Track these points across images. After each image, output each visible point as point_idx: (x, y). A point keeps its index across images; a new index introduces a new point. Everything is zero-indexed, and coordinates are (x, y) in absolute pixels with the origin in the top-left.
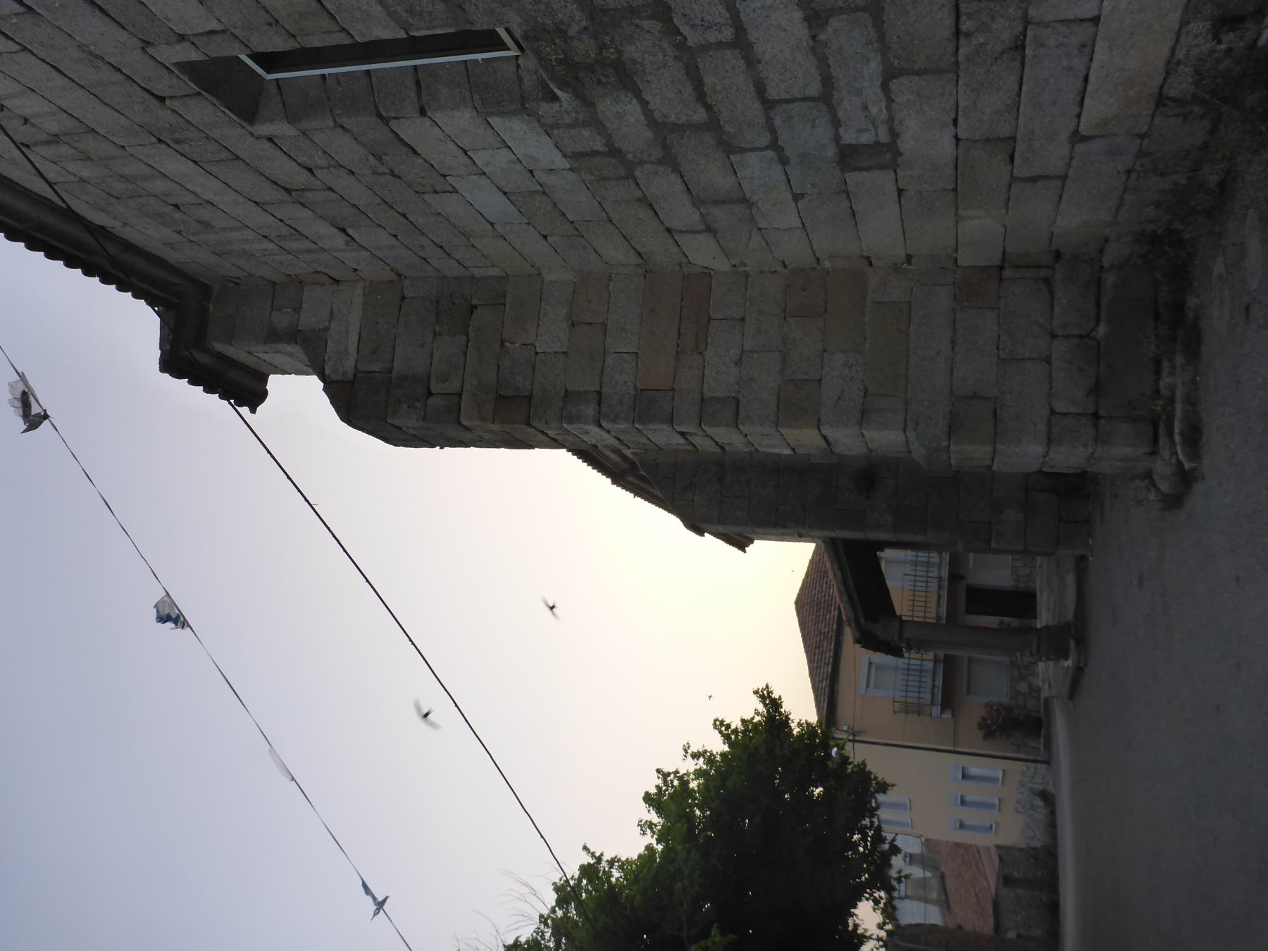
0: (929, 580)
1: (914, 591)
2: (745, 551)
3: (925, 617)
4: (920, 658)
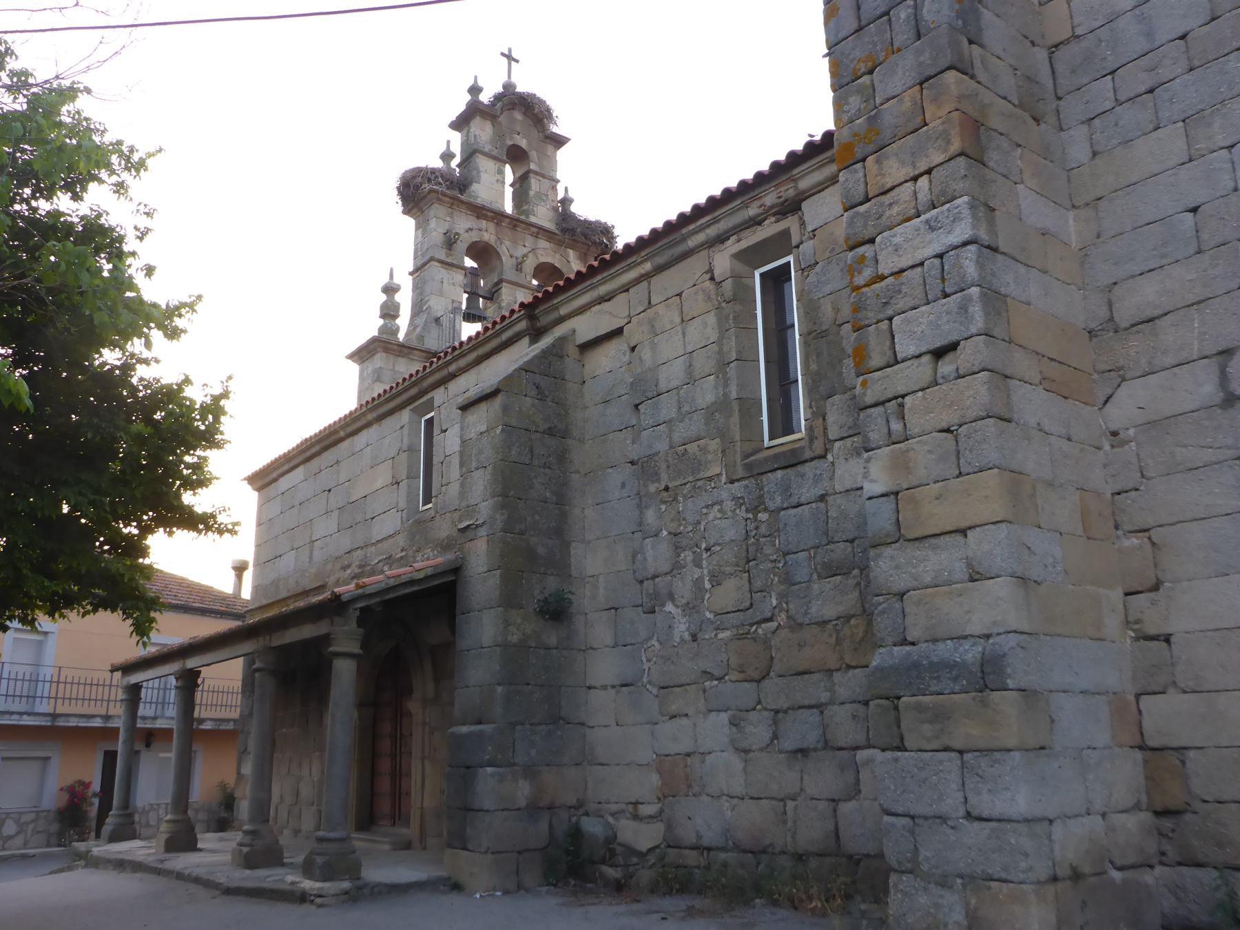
0: (105, 704)
1: (218, 692)
2: (245, 479)
3: (201, 705)
4: (59, 696)
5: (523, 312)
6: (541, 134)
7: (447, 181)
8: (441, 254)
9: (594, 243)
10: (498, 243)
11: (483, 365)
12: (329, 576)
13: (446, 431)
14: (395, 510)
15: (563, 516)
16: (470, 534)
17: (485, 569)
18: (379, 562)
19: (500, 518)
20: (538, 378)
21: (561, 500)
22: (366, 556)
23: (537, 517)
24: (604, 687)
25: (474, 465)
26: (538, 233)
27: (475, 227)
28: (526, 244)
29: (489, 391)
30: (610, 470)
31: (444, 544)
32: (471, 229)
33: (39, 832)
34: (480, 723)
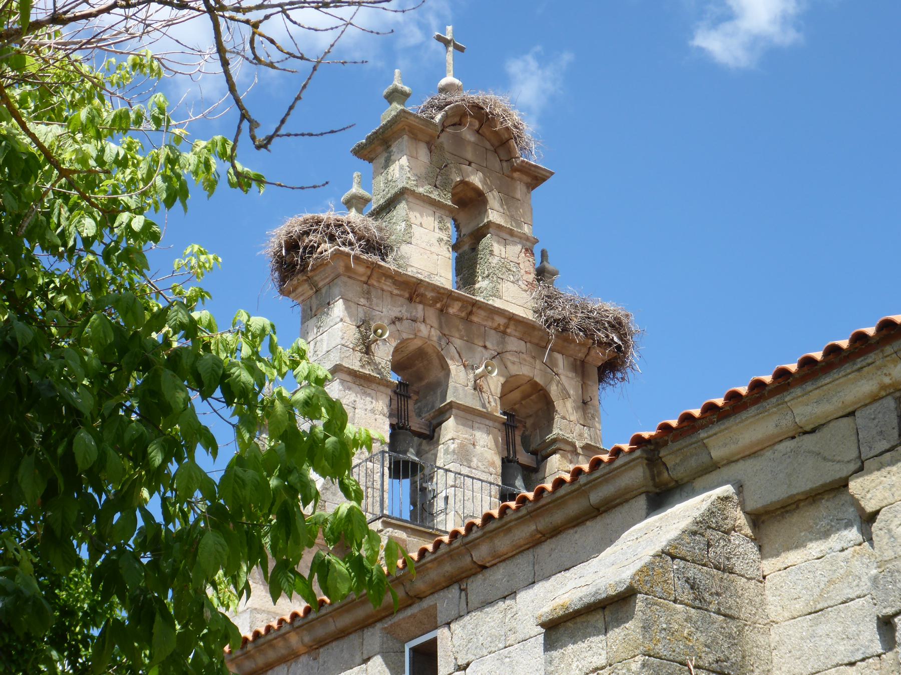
5: (638, 453)
6: (505, 164)
7: (359, 239)
8: (354, 362)
9: (600, 343)
10: (443, 343)
11: (546, 548)
20: (693, 571)
26: (507, 326)
27: (406, 315)
28: (488, 345)
29: (612, 592)
32: (399, 319)
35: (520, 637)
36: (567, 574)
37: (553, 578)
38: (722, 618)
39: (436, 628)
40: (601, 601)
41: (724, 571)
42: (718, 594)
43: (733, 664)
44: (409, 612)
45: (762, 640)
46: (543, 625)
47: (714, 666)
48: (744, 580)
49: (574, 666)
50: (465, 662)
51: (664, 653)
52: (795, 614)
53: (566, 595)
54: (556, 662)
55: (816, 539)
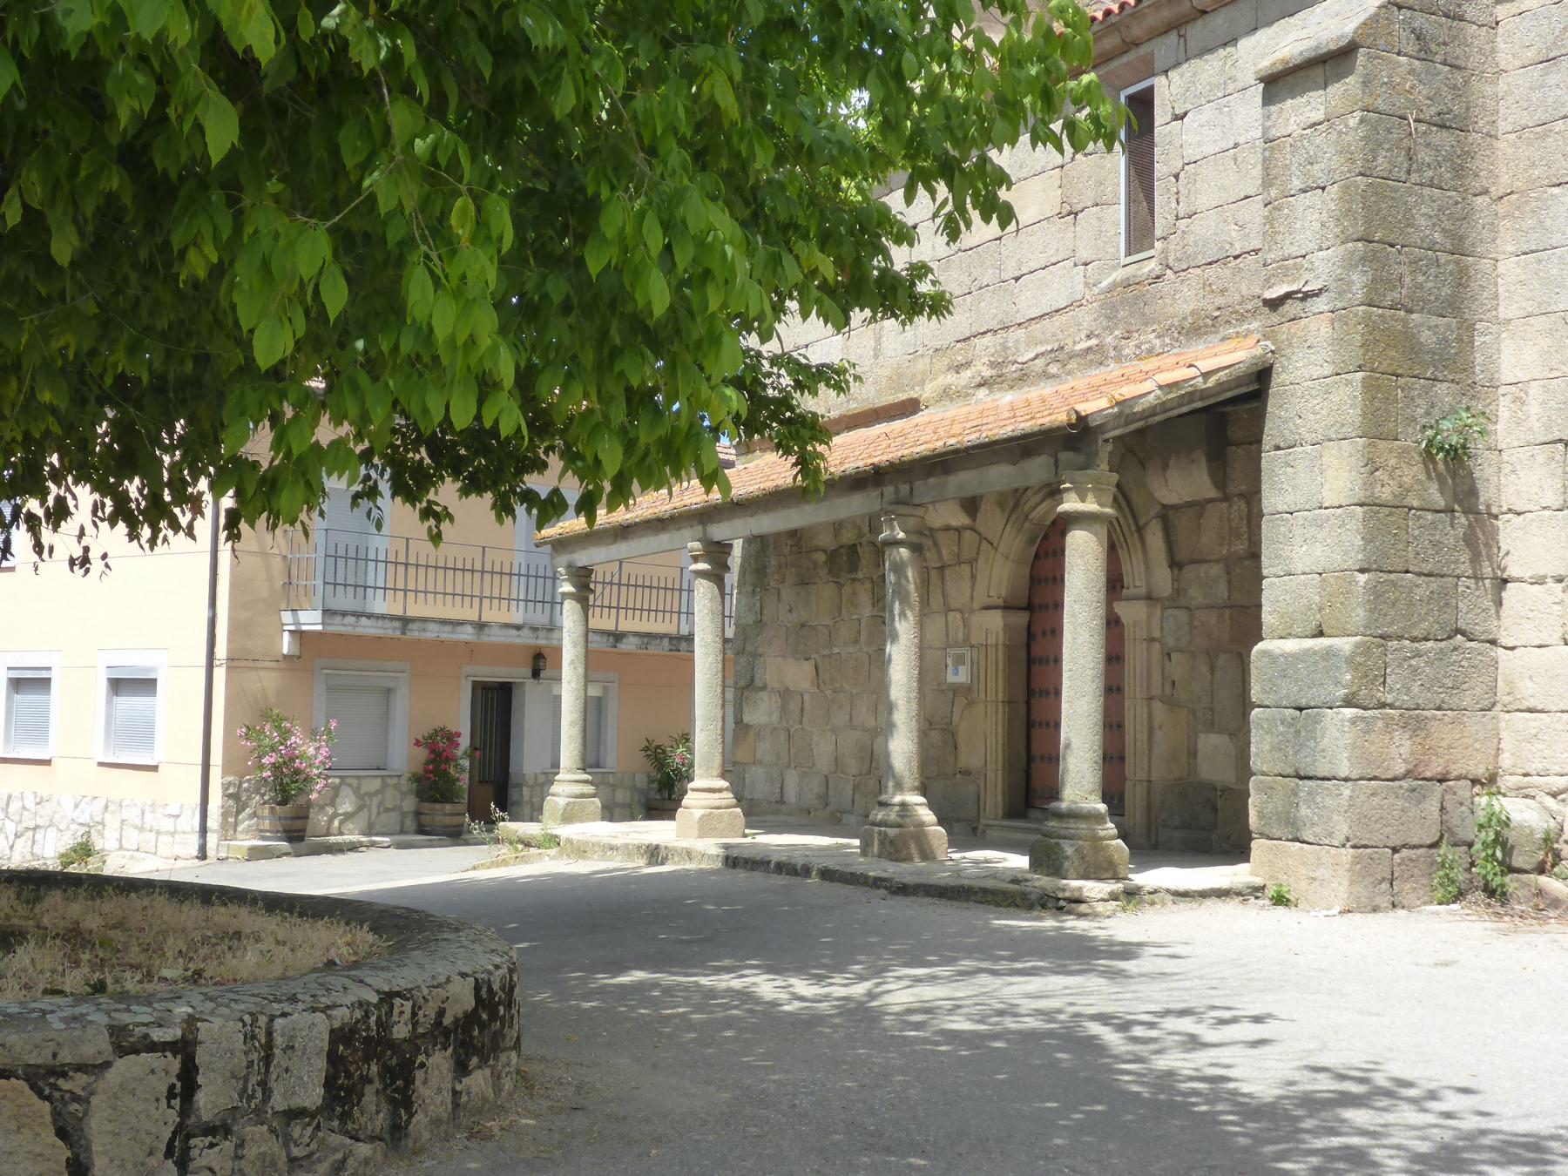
12: (923, 383)
13: (1181, 117)
14: (1069, 263)
15: (1462, 277)
16: (1291, 308)
17: (1328, 370)
18: (1036, 357)
19: (1359, 280)
20: (1420, 21)
21: (1459, 248)
22: (1005, 348)
23: (1421, 279)
24: (1539, 581)
25: (1297, 183)
29: (1333, 47)
30: (1556, 190)
31: (1186, 324)
33: (387, 810)
34: (1321, 634)
35: (1240, 85)
36: (1291, 20)
37: (1276, 24)
38: (1448, 68)
39: (1153, 75)
40: (1321, 56)
41: (1454, 19)
42: (1445, 44)
43: (1456, 116)
44: (1125, 59)
45: (1489, 90)
46: (1261, 80)
47: (1436, 119)
48: (1475, 27)
49: (1292, 121)
50: (1183, 111)
51: (1382, 107)
52: (1527, 62)
53: (1288, 48)
54: (1274, 117)
55: (1059, 428)
